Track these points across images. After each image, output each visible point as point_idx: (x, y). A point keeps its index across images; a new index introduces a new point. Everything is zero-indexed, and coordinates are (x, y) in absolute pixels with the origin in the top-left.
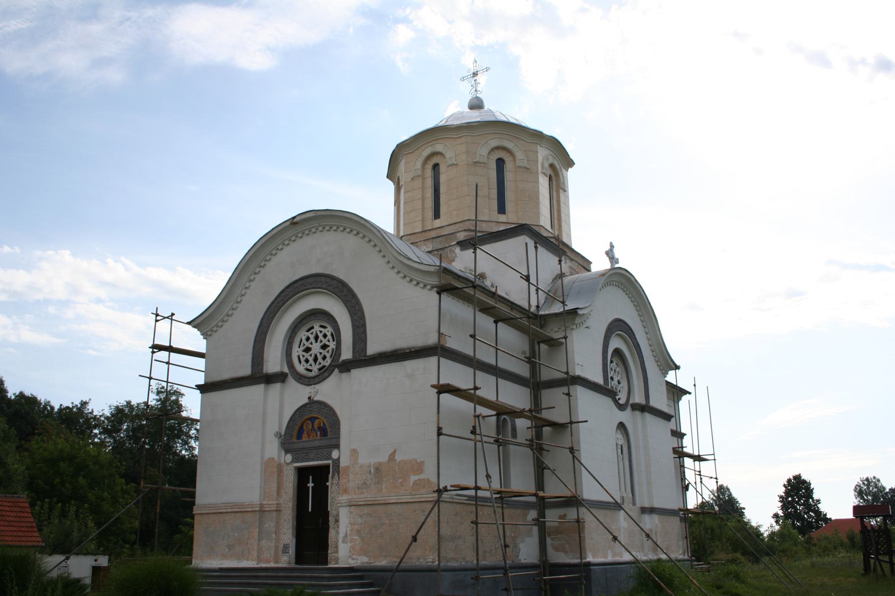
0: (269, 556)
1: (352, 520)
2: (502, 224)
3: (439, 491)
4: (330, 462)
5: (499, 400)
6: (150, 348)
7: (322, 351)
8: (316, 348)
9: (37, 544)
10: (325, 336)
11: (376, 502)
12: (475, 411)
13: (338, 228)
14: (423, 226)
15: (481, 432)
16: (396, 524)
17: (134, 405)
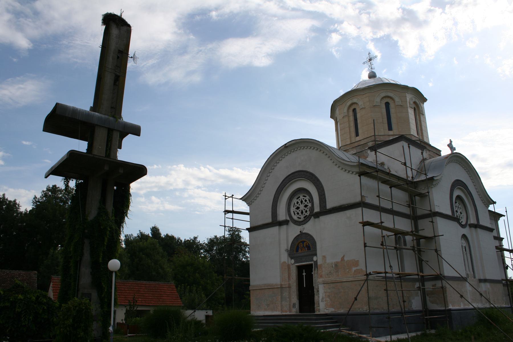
0: (286, 309)
1: (325, 290)
2: (391, 136)
3: (367, 275)
4: (313, 262)
5: (395, 227)
6: (223, 212)
7: (305, 208)
8: (302, 207)
9: (181, 305)
10: (306, 201)
12: (382, 234)
13: (307, 147)
14: (351, 141)
15: (386, 245)
17: (218, 237)
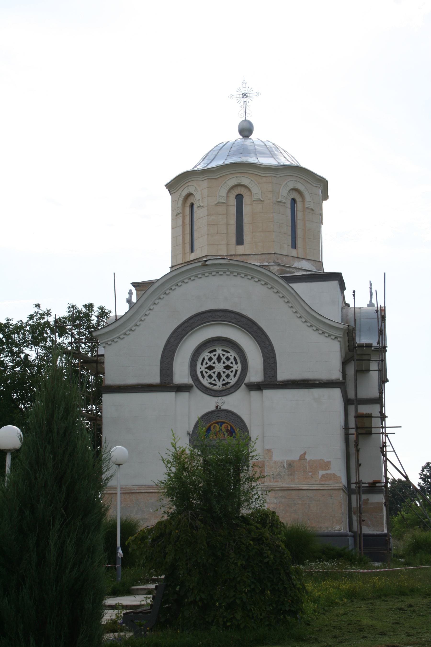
10: (228, 359)
11: (291, 488)
16: (307, 504)
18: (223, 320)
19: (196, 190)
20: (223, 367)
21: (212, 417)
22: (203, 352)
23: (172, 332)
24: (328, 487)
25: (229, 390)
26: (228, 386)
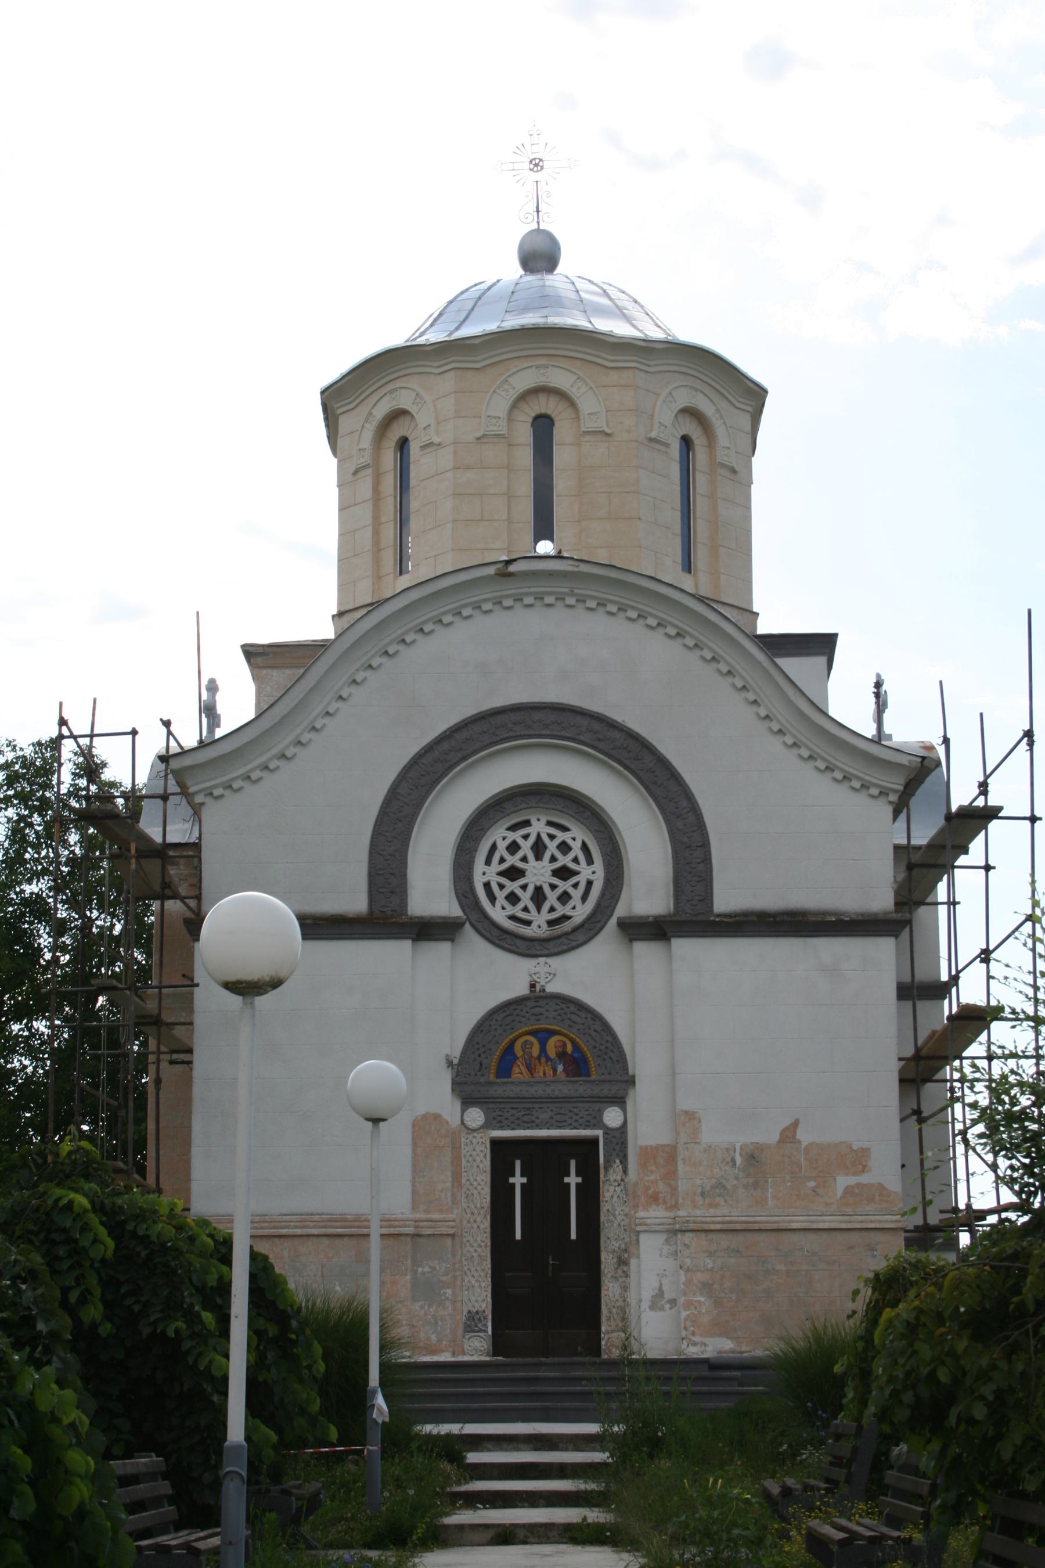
0: (434, 1337)
4: (599, 1133)
10: (564, 848)
11: (756, 1226)
16: (804, 1273)
18: (554, 733)
19: (418, 400)
20: (550, 873)
21: (518, 1015)
22: (493, 827)
23: (406, 766)
24: (862, 1222)
25: (568, 939)
26: (567, 926)
